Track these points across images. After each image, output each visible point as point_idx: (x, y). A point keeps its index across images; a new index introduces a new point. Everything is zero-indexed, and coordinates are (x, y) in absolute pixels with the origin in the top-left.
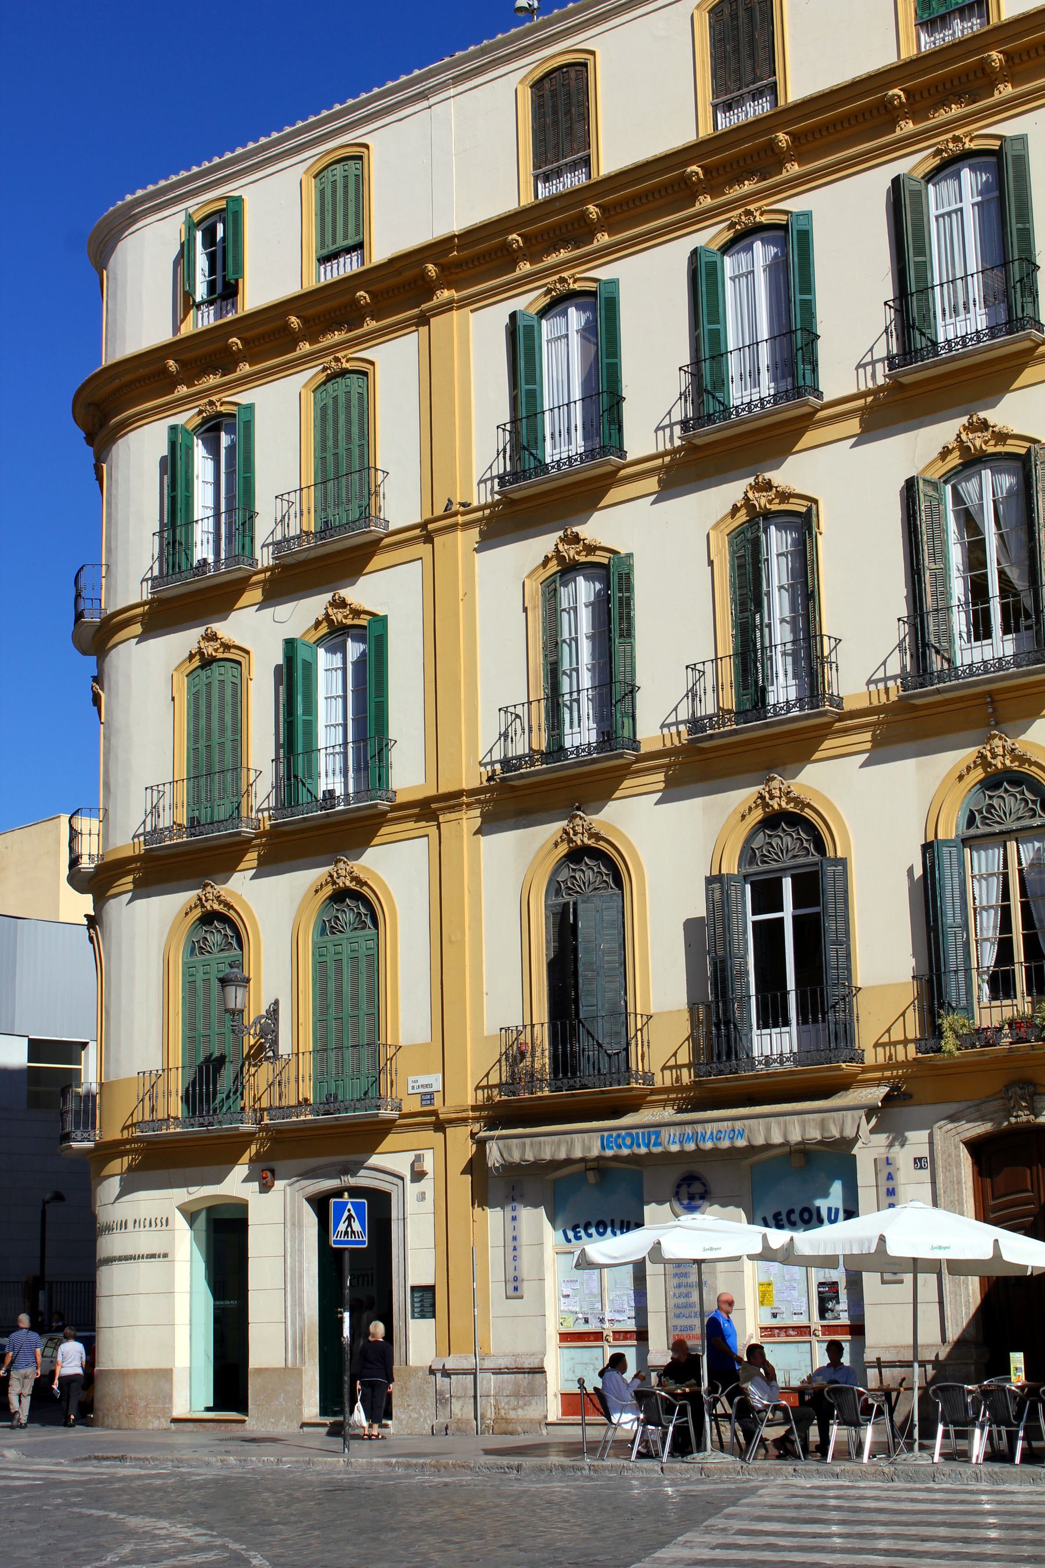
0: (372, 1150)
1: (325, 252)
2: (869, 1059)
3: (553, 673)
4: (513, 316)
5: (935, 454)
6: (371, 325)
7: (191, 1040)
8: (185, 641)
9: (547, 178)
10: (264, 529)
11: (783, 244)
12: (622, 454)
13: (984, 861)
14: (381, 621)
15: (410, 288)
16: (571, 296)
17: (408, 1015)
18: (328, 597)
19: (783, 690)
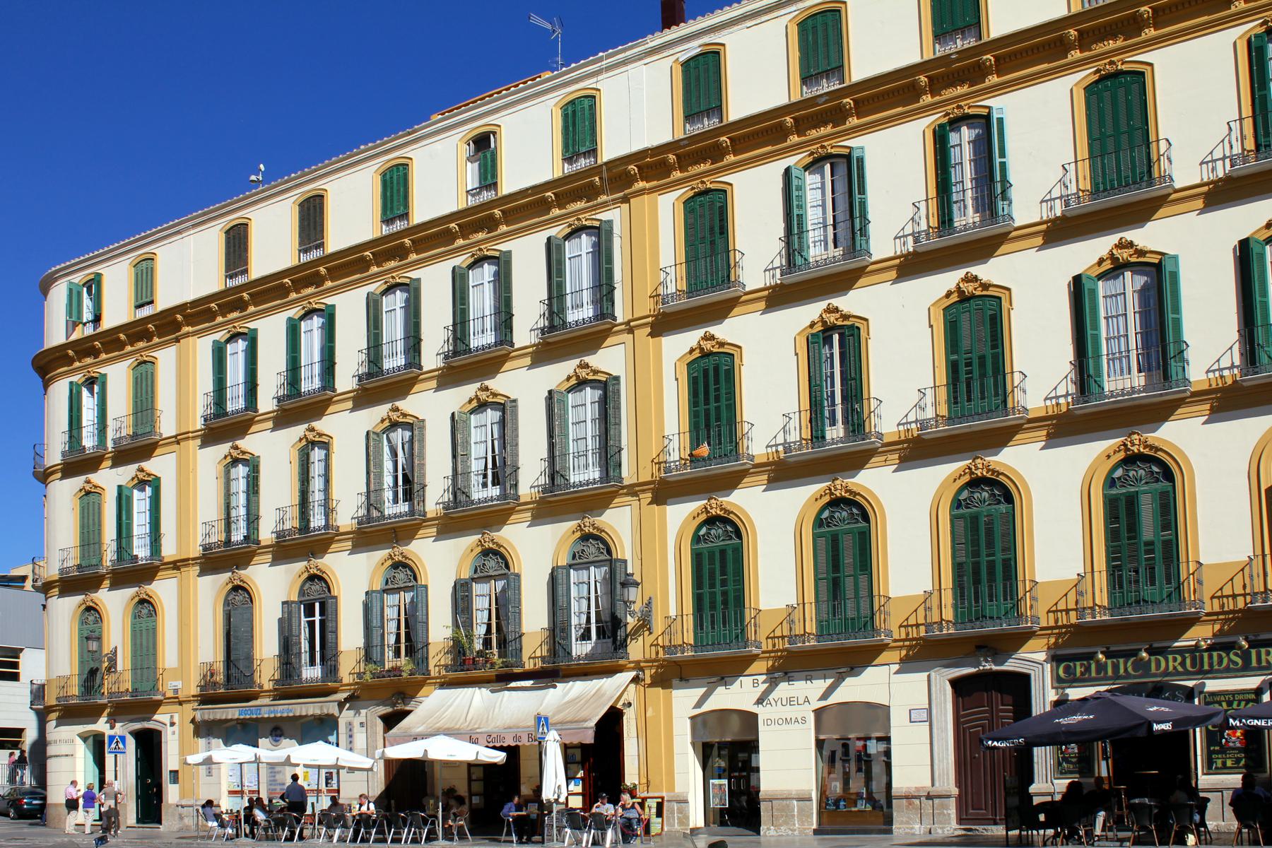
0: (154, 713)
1: (140, 302)
2: (346, 681)
3: (228, 508)
4: (549, 239)
5: (944, 294)
6: (413, 257)
7: (82, 663)
8: (77, 482)
9: (231, 277)
10: (111, 434)
11: (599, 237)
12: (512, 345)
13: (391, 600)
14: (158, 479)
15: (170, 325)
16: (398, 285)
17: (168, 656)
18: (577, 361)
19: (317, 521)
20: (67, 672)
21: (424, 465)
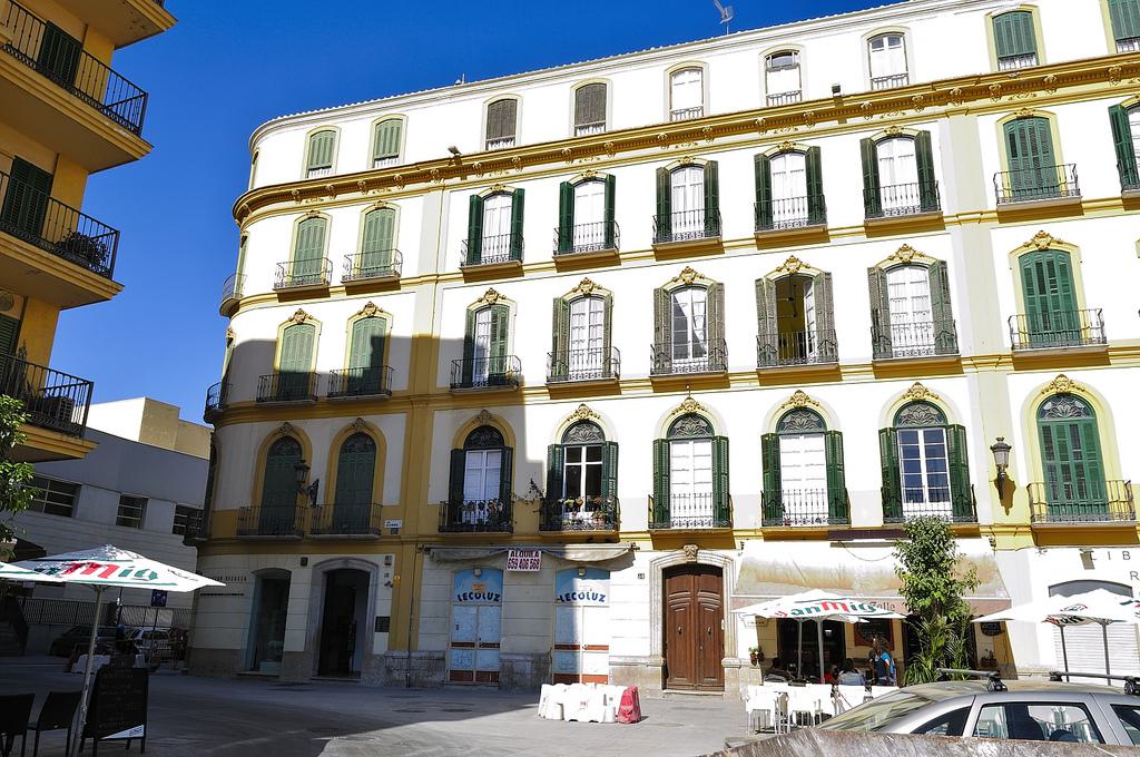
9: (581, 128)
17: (389, 489)
20: (246, 502)
21: (723, 324)
